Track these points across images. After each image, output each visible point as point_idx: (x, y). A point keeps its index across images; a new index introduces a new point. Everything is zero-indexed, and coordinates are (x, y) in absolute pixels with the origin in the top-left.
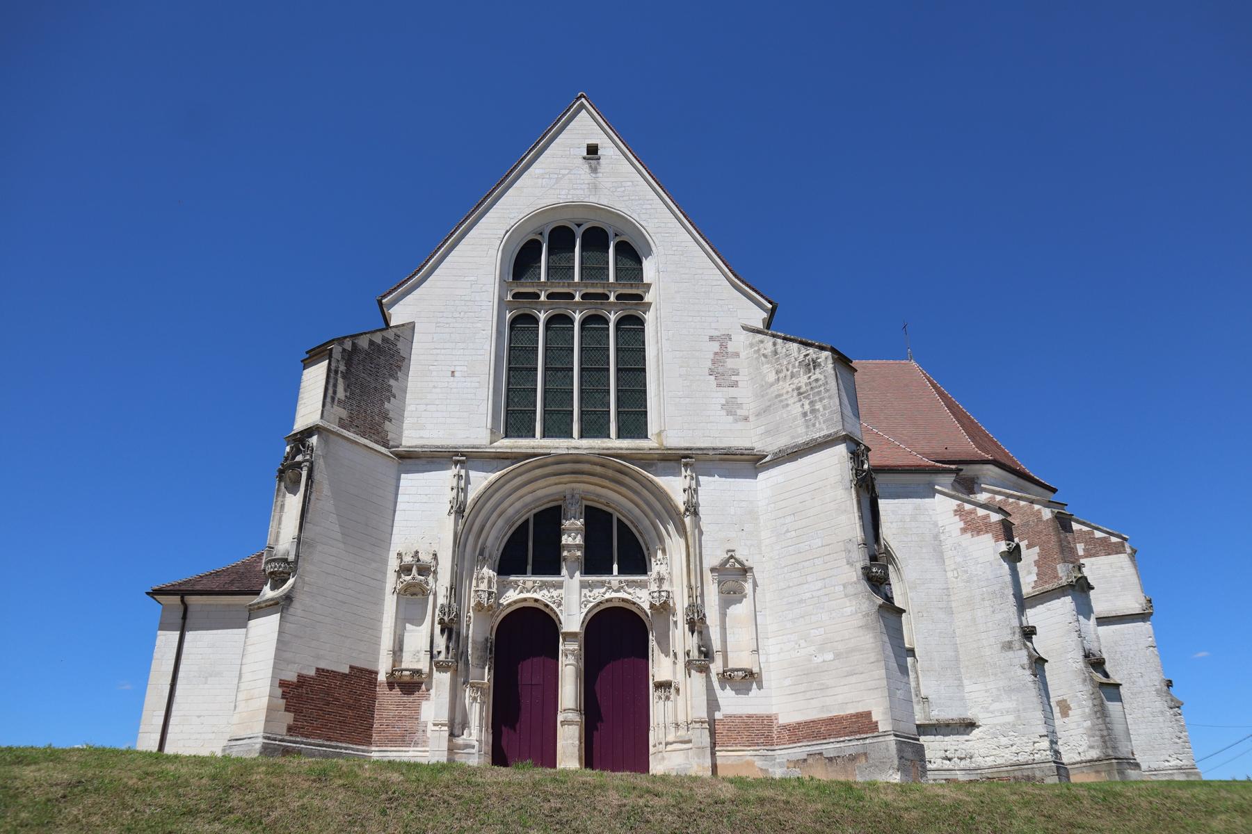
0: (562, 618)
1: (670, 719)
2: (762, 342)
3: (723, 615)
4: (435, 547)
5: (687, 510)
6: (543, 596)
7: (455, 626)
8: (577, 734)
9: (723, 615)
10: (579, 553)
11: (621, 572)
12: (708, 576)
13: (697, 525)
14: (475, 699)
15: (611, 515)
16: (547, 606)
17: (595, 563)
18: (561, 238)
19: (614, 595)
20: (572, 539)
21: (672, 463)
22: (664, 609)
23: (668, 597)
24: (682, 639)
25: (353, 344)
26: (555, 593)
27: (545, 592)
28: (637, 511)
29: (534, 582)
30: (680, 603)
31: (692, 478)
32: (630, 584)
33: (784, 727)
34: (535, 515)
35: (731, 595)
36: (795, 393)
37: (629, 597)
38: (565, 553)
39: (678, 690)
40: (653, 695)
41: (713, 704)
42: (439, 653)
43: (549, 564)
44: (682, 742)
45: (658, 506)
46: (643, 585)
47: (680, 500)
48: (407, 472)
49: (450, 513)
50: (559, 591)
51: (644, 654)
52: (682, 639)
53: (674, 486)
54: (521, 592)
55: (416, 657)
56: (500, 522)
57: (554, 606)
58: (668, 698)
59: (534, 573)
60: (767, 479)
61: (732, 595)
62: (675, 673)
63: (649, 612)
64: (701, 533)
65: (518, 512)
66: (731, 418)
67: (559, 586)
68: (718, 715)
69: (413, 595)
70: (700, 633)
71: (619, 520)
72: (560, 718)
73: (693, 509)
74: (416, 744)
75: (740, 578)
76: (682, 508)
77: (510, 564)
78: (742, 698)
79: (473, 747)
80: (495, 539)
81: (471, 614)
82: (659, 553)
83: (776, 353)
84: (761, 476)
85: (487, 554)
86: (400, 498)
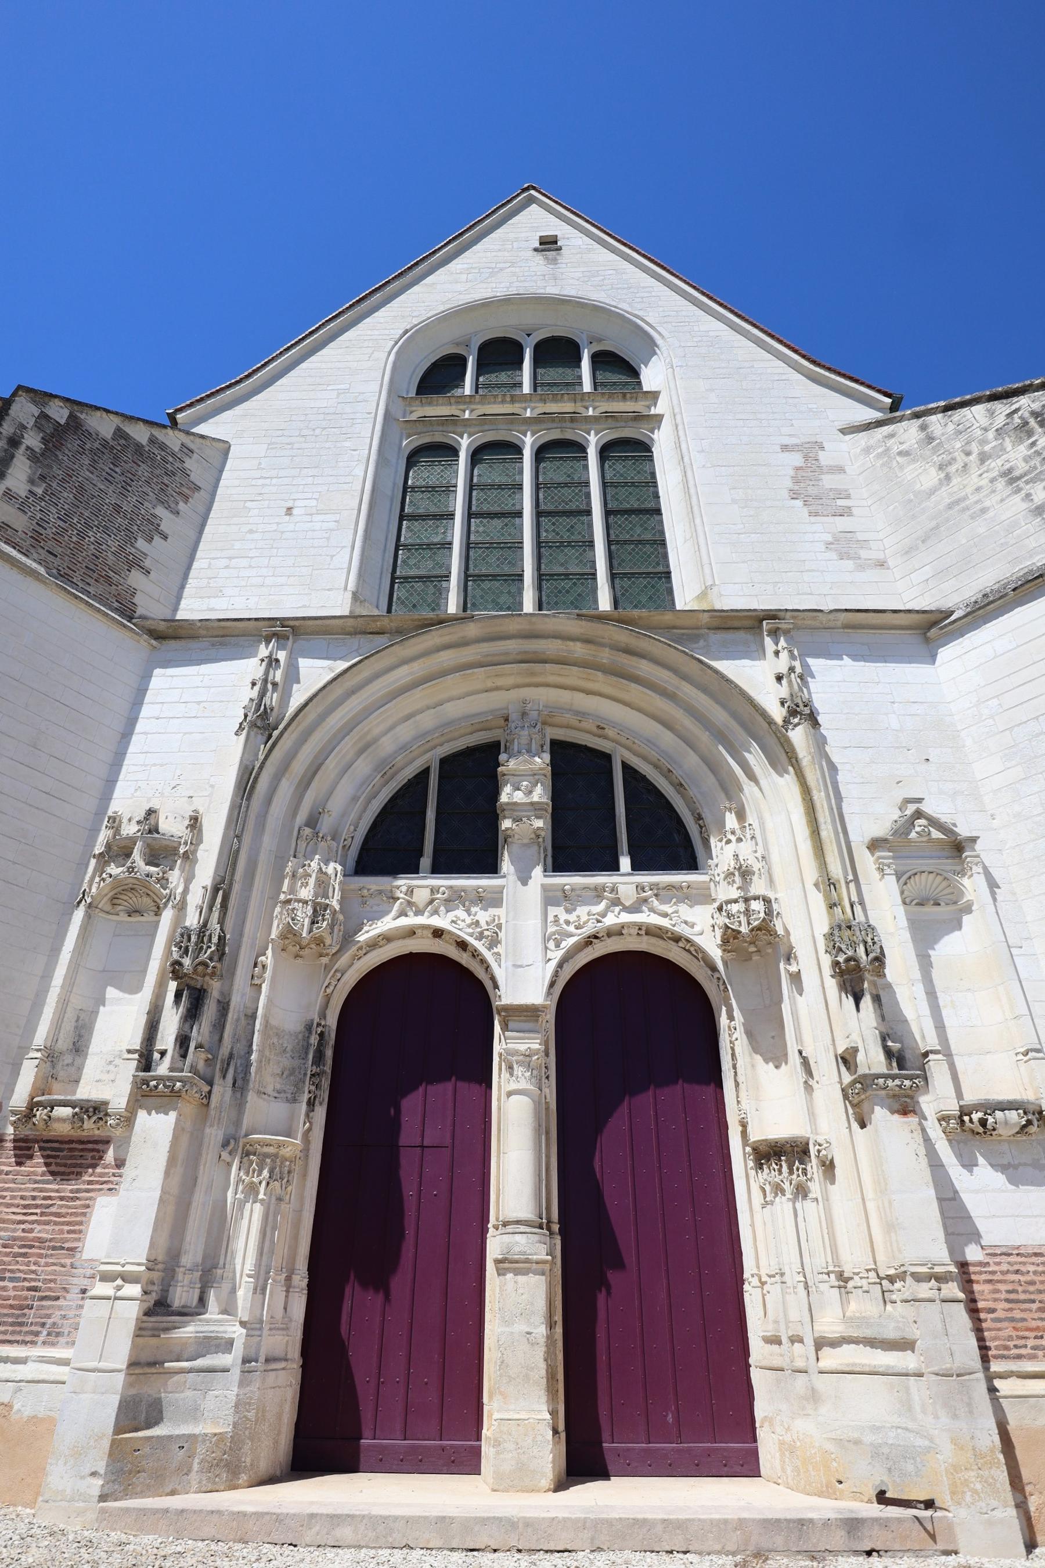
2: (892, 436)
4: (199, 805)
5: (793, 712)
6: (454, 921)
7: (215, 988)
10: (539, 823)
11: (636, 867)
12: (866, 862)
13: (820, 743)
14: (252, 1190)
15: (607, 757)
16: (463, 945)
17: (578, 845)
18: (499, 354)
19: (626, 918)
20: (525, 791)
22: (758, 943)
23: (769, 912)
25: (72, 416)
26: (483, 916)
27: (460, 913)
28: (667, 739)
29: (434, 890)
30: (805, 924)
31: (792, 657)
32: (661, 892)
34: (443, 761)
35: (935, 911)
36: (1001, 484)
37: (664, 922)
38: (506, 824)
39: (829, 1167)
40: (747, 1183)
42: (163, 1053)
43: (473, 850)
44: (872, 1343)
45: (719, 715)
47: (771, 699)
50: (493, 911)
52: (818, 1014)
54: (403, 913)
56: (363, 767)
57: (479, 946)
59: (437, 869)
62: (812, 1114)
63: (716, 953)
64: (833, 768)
66: (849, 564)
67: (494, 900)
68: (973, 1254)
69: (133, 912)
70: (877, 999)
71: (625, 766)
72: (495, 1245)
73: (801, 711)
75: (948, 865)
76: (778, 714)
77: (387, 848)
79: (228, 1345)
80: (352, 800)
81: (268, 959)
82: (731, 821)
83: (930, 439)
84: (945, 653)
85: (326, 825)
86: (146, 711)
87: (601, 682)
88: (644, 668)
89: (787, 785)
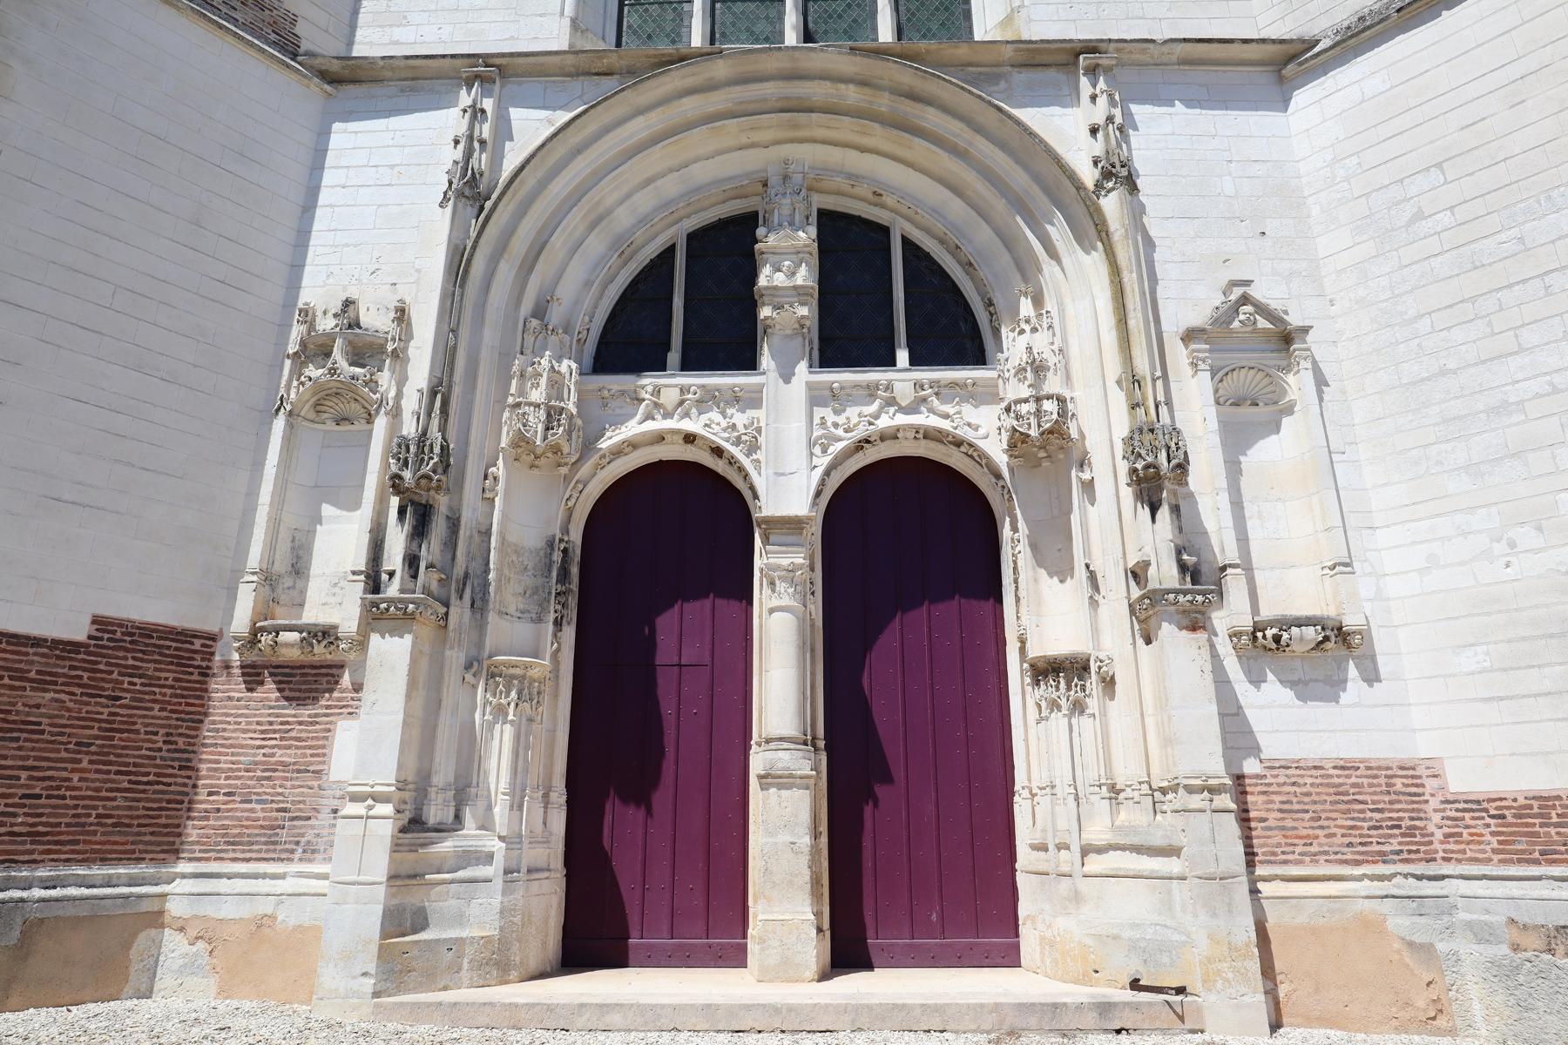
0: (759, 482)
1: (1091, 772)
3: (1234, 470)
5: (1107, 175)
6: (710, 425)
8: (805, 816)
9: (1234, 470)
10: (803, 311)
11: (915, 361)
12: (1178, 355)
13: (1137, 213)
14: (501, 711)
15: (885, 231)
16: (718, 451)
17: (849, 338)
19: (902, 419)
20: (787, 273)
21: (1051, 74)
22: (1049, 448)
23: (1063, 413)
24: (1111, 527)
26: (740, 419)
29: (684, 390)
30: (1103, 426)
31: (1112, 103)
32: (942, 391)
33: (1475, 805)
34: (692, 237)
35: (1250, 411)
37: (945, 425)
38: (765, 312)
39: (1109, 683)
40: (1023, 697)
41: (1236, 732)
43: (727, 341)
44: (1138, 849)
45: (1019, 178)
46: (988, 395)
47: (1081, 156)
48: (347, 117)
49: (446, 198)
50: (751, 413)
51: (988, 584)
53: (1068, 128)
54: (649, 417)
55: (331, 598)
56: (596, 245)
57: (736, 451)
58: (1078, 707)
59: (687, 365)
60: (1318, 102)
61: (1246, 411)
62: (1095, 631)
63: (1001, 459)
64: (1150, 244)
65: (643, 221)
67: (752, 400)
68: (1250, 767)
69: (341, 420)
70: (1176, 509)
71: (907, 243)
72: (758, 762)
74: (310, 852)
75: (1271, 359)
76: (1089, 176)
78: (1318, 711)
79: (489, 858)
80: (586, 287)
82: (1026, 307)
85: (555, 315)
86: (329, 178)
87: (878, 136)
88: (932, 118)
89: (1093, 264)
